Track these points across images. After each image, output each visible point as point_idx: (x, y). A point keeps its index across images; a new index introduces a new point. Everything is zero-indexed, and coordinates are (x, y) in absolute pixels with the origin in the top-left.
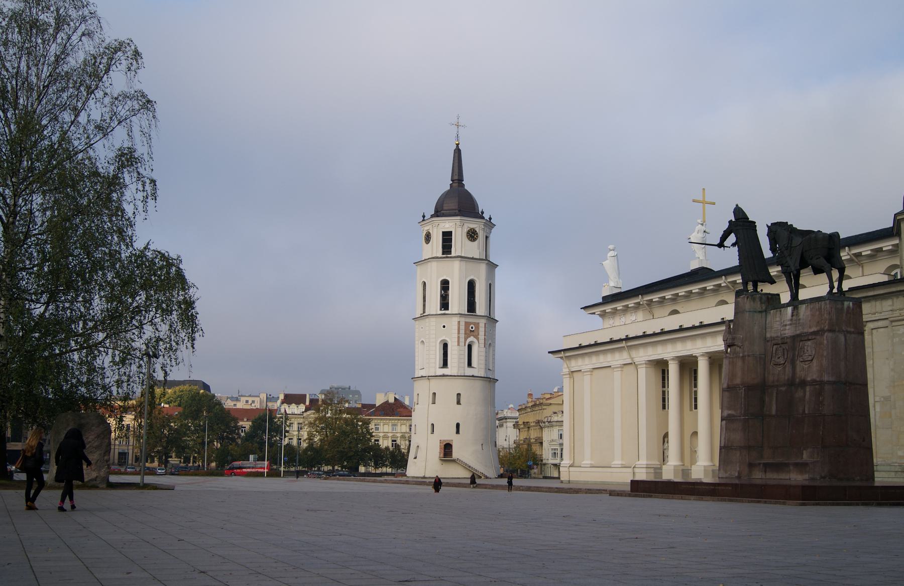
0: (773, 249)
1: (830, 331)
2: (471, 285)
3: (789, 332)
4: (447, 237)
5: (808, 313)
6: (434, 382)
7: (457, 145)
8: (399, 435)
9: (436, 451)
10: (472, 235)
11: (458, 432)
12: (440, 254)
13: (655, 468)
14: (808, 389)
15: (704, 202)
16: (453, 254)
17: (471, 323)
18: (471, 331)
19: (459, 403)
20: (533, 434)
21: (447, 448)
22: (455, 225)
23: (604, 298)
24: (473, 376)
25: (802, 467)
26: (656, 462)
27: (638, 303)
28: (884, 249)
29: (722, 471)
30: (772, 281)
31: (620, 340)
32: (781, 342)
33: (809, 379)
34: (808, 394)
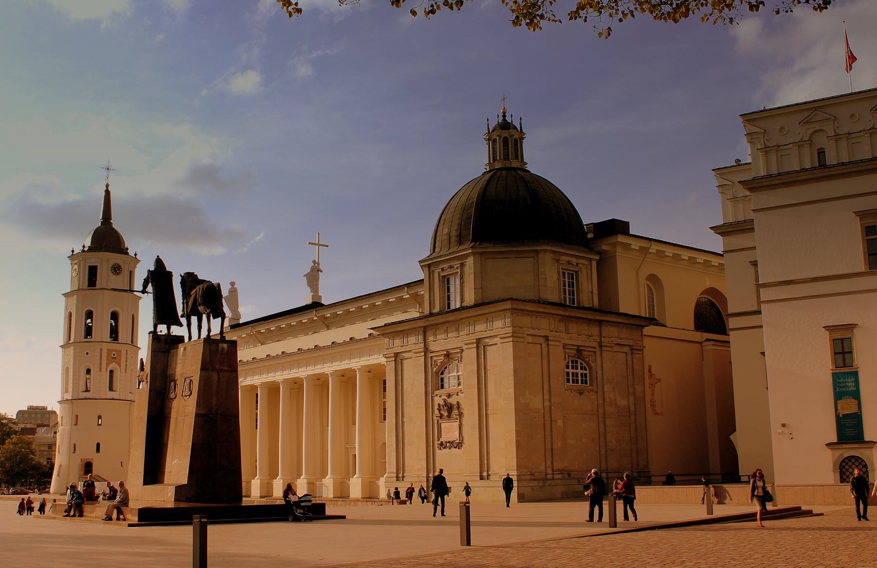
7: (107, 186)
17: (113, 350)
30: (181, 325)
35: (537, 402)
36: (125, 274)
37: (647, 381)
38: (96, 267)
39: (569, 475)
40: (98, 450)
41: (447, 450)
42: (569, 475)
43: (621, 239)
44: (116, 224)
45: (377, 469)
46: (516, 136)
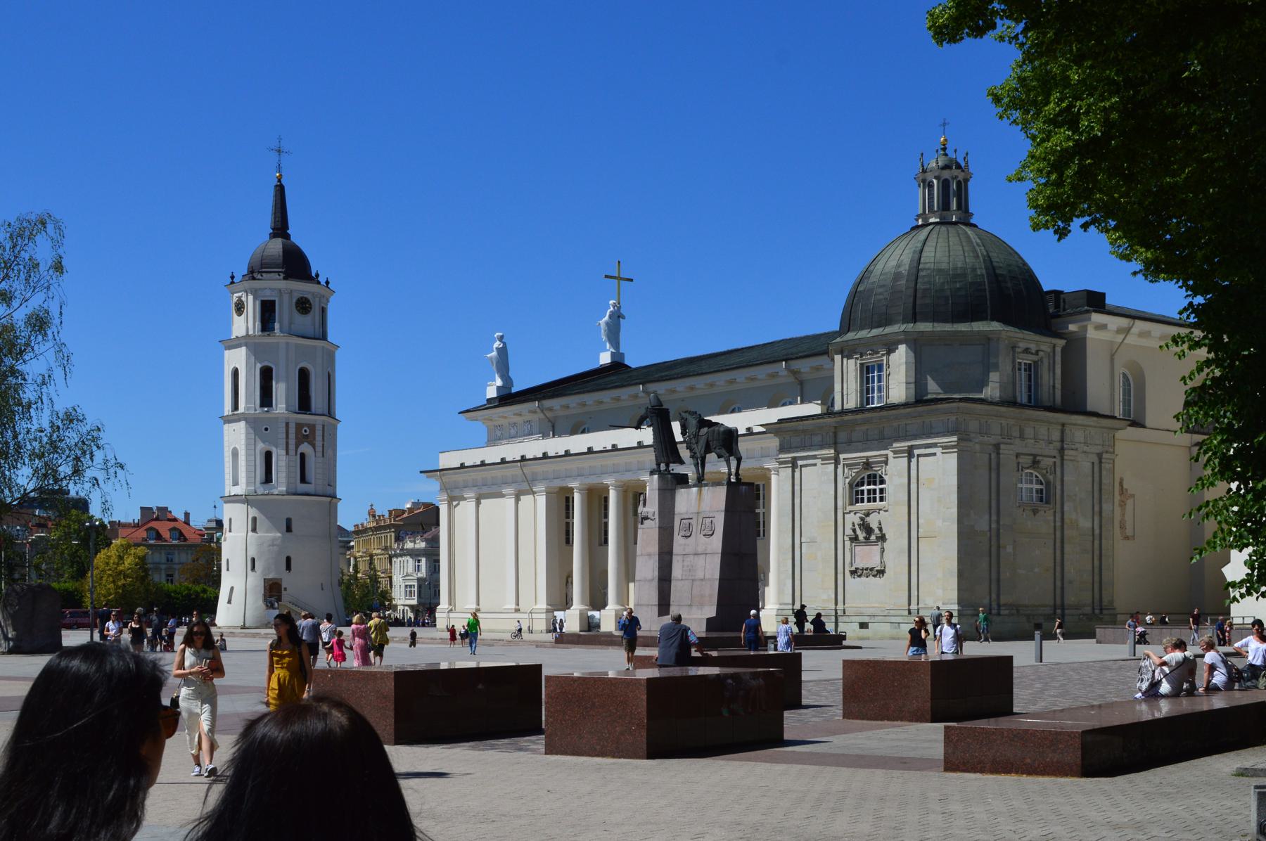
0: (683, 433)
22: (275, 285)
23: (489, 401)
30: (682, 462)
35: (982, 524)
36: (316, 311)
37: (1117, 498)
38: (273, 302)
39: (1018, 611)
40: (288, 567)
41: (863, 579)
42: (1018, 611)
43: (1097, 318)
44: (298, 235)
45: (597, 599)
46: (961, 176)
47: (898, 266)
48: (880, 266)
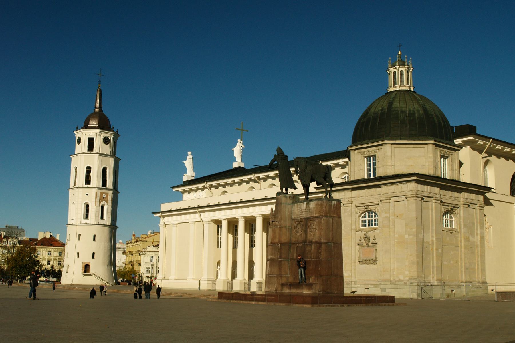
1: (326, 216)
2: (105, 170)
3: (304, 215)
4: (91, 141)
5: (315, 206)
6: (79, 227)
8: (52, 258)
9: (80, 269)
10: (106, 141)
11: (93, 257)
12: (86, 151)
13: (212, 281)
14: (313, 246)
15: (242, 130)
16: (94, 152)
17: (103, 193)
18: (102, 198)
19: (94, 240)
20: (135, 258)
21: (87, 268)
23: (184, 182)
24: (104, 225)
25: (310, 286)
26: (213, 277)
27: (204, 186)
28: (340, 164)
29: (267, 288)
31: (195, 208)
32: (299, 221)
33: (314, 241)
34: (313, 248)
38: (93, 139)
47: (382, 109)
48: (372, 110)
